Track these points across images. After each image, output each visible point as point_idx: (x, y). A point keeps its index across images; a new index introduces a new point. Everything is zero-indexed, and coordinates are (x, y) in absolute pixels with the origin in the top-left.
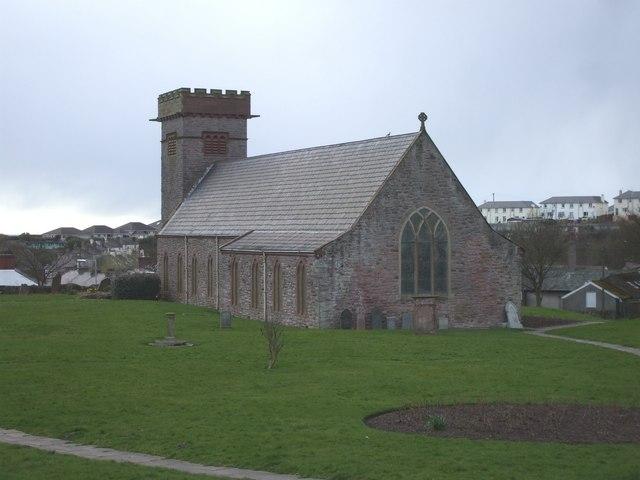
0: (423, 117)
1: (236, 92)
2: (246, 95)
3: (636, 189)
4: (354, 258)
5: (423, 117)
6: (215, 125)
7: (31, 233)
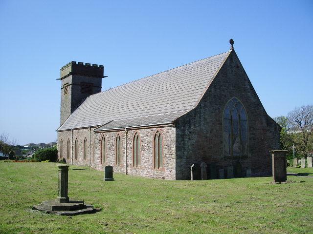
0: (232, 42)
1: (97, 65)
2: (102, 68)
3: (2, 164)
4: (197, 128)
5: (232, 42)
6: (87, 79)
7: (47, 143)
